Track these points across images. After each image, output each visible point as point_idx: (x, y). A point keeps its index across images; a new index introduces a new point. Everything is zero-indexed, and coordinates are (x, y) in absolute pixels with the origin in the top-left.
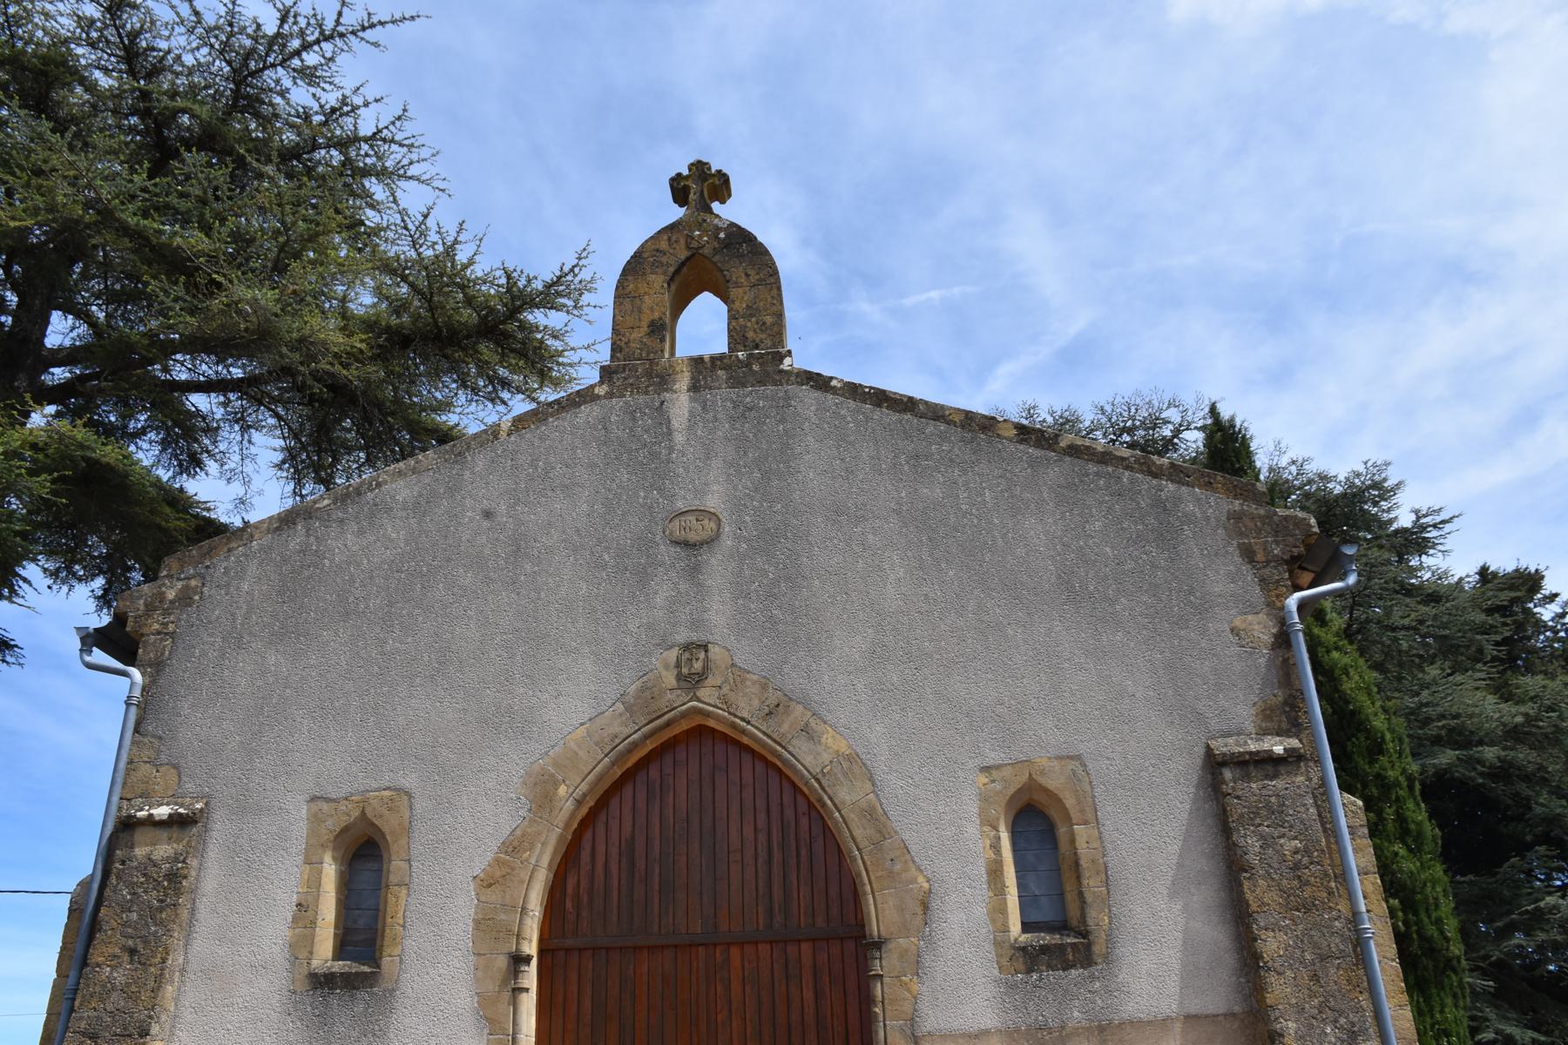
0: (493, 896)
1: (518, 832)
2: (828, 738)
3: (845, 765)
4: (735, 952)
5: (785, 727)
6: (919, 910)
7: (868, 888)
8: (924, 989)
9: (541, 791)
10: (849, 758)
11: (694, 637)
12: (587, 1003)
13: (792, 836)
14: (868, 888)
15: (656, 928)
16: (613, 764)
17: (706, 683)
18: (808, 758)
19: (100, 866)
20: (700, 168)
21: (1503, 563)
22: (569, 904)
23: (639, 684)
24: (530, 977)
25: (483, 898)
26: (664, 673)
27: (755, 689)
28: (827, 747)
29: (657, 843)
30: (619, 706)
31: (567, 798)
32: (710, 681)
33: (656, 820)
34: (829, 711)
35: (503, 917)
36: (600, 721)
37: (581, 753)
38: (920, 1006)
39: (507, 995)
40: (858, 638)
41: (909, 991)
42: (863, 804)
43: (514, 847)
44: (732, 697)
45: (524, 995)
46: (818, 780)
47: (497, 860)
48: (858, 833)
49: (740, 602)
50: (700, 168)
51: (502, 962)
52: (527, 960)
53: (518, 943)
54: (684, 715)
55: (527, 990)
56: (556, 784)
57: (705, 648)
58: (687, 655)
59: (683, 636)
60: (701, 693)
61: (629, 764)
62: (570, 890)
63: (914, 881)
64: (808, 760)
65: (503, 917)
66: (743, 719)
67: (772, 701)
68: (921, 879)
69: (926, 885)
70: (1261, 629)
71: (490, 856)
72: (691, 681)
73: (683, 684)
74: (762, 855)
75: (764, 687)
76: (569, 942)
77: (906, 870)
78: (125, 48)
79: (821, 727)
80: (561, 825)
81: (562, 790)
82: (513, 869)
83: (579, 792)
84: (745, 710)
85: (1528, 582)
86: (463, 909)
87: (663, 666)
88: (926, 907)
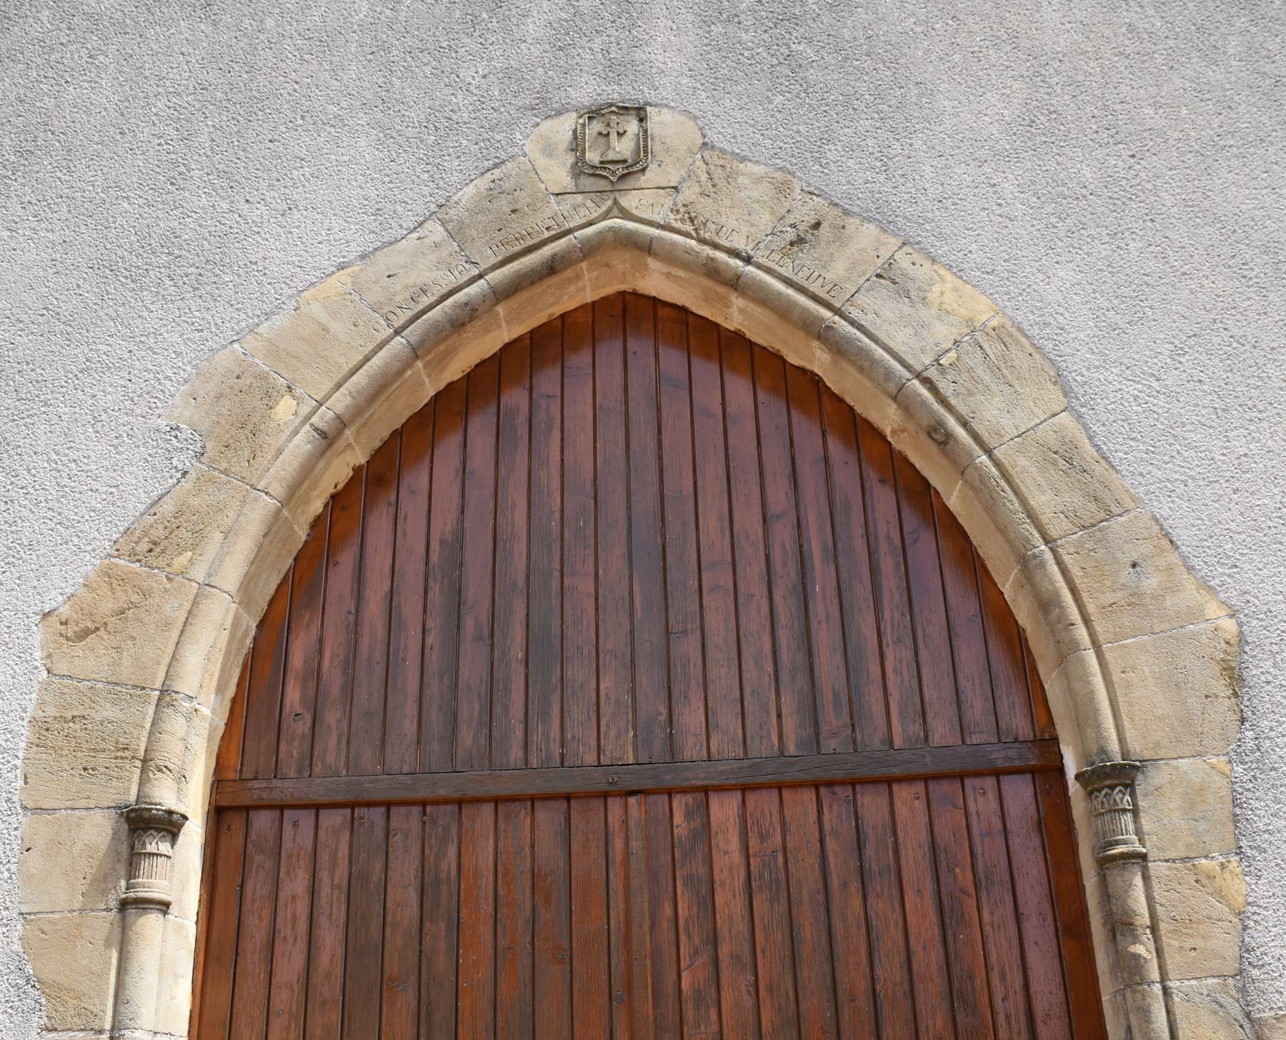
0: (89, 661)
1: (168, 507)
2: (945, 289)
3: (993, 349)
4: (724, 810)
5: (837, 270)
6: (1220, 687)
7: (1081, 633)
8: (1262, 888)
10: (999, 334)
11: (614, 93)
12: (330, 938)
13: (858, 531)
14: (1081, 633)
15: (516, 752)
16: (416, 352)
17: (643, 180)
19: (204, 903)
22: (293, 696)
23: (483, 183)
24: (179, 871)
25: (62, 667)
26: (541, 162)
27: (763, 192)
28: (943, 312)
29: (520, 548)
30: (435, 231)
32: (653, 176)
33: (516, 495)
34: (942, 237)
35: (109, 711)
36: (385, 261)
37: (336, 327)
38: (1257, 936)
39: (104, 921)
40: (993, 97)
41: (1220, 895)
42: (1046, 433)
43: (155, 543)
44: (705, 208)
45: (151, 921)
46: (927, 382)
47: (108, 575)
48: (1041, 501)
49: (717, 29)
51: (98, 830)
52: (170, 825)
53: (143, 781)
54: (590, 250)
55: (164, 907)
56: (270, 398)
57: (640, 113)
58: (597, 126)
59: (587, 91)
60: (629, 201)
61: (456, 369)
62: (297, 659)
63: (1196, 614)
64: (900, 339)
65: (109, 711)
66: (734, 253)
67: (804, 213)
68: (1213, 610)
69: (1230, 626)
71: (89, 565)
73: (588, 183)
74: (786, 575)
75: (783, 189)
76: (287, 789)
77: (1175, 589)
79: (924, 271)
80: (278, 489)
81: (285, 409)
82: (145, 594)
83: (323, 418)
87: (544, 152)
88: (1235, 678)
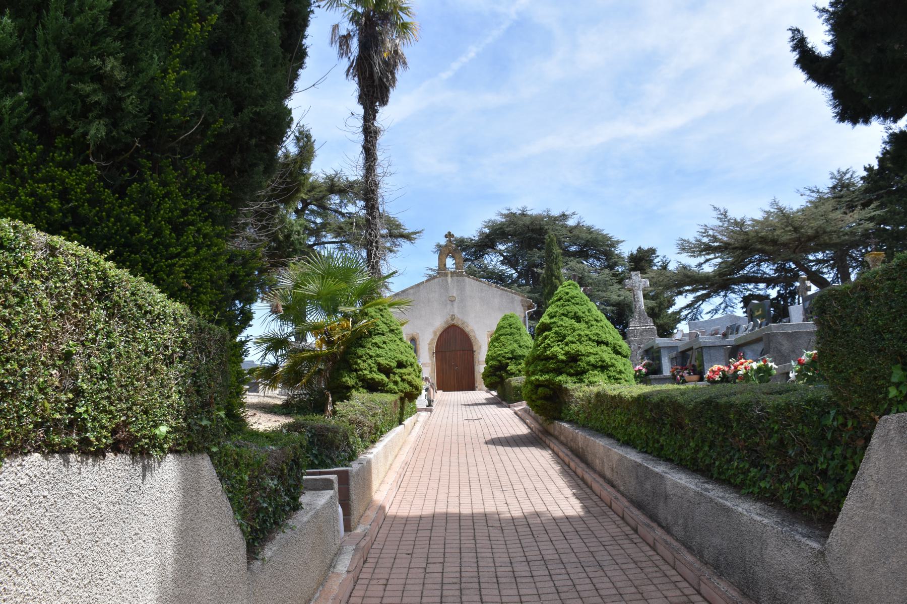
9: (435, 333)
18: (467, 330)
20: (449, 233)
21: (645, 247)
31: (438, 334)
43: (432, 340)
50: (449, 233)
70: (523, 315)
72: (452, 320)
78: (370, 228)
84: (459, 324)
85: (652, 251)
86: (427, 347)
87: (449, 317)
